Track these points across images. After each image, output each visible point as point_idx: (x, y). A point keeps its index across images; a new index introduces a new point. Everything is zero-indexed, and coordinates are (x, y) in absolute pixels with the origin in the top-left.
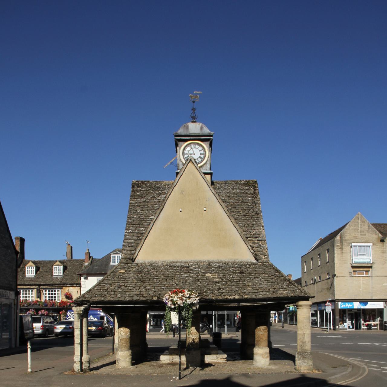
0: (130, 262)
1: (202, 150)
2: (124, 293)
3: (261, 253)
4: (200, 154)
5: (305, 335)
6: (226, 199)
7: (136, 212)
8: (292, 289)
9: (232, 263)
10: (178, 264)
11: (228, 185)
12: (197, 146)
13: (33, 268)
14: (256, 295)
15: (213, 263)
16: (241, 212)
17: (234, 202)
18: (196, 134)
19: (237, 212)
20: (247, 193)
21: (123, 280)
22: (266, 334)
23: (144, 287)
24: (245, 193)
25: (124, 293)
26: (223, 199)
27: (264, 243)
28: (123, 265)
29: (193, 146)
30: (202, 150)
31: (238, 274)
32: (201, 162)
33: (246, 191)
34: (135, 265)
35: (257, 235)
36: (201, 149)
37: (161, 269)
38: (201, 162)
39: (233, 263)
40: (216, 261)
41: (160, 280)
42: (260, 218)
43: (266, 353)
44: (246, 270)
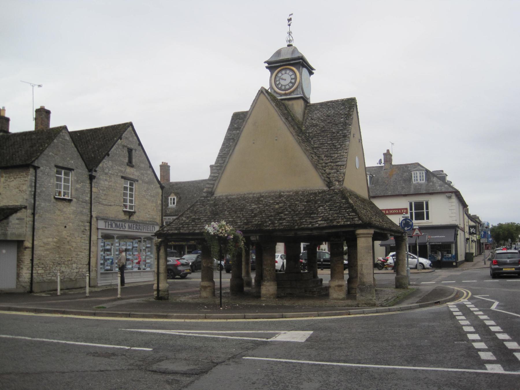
0: (209, 195)
1: (293, 74)
2: (196, 226)
3: (336, 179)
4: (290, 79)
5: (363, 266)
6: (318, 122)
7: (228, 145)
8: (351, 217)
9: (302, 192)
10: (251, 196)
11: (323, 107)
12: (288, 71)
13: (415, 181)
14: (313, 225)
15: (284, 192)
16: (329, 136)
17: (325, 125)
18: (285, 60)
19: (324, 136)
20: (341, 114)
21: (199, 213)
22: (156, 263)
23: (332, 215)
24: (339, 113)
25: (196, 226)
26: (315, 122)
27: (342, 168)
28: (203, 198)
29: (283, 72)
30: (293, 74)
31: (304, 203)
32: (292, 87)
33: (341, 112)
34: (213, 198)
35: (338, 160)
36: (292, 74)
37: (235, 201)
38: (293, 87)
39: (303, 192)
40: (288, 190)
41: (230, 212)
42: (347, 140)
43: (29, 273)
44: (314, 198)
